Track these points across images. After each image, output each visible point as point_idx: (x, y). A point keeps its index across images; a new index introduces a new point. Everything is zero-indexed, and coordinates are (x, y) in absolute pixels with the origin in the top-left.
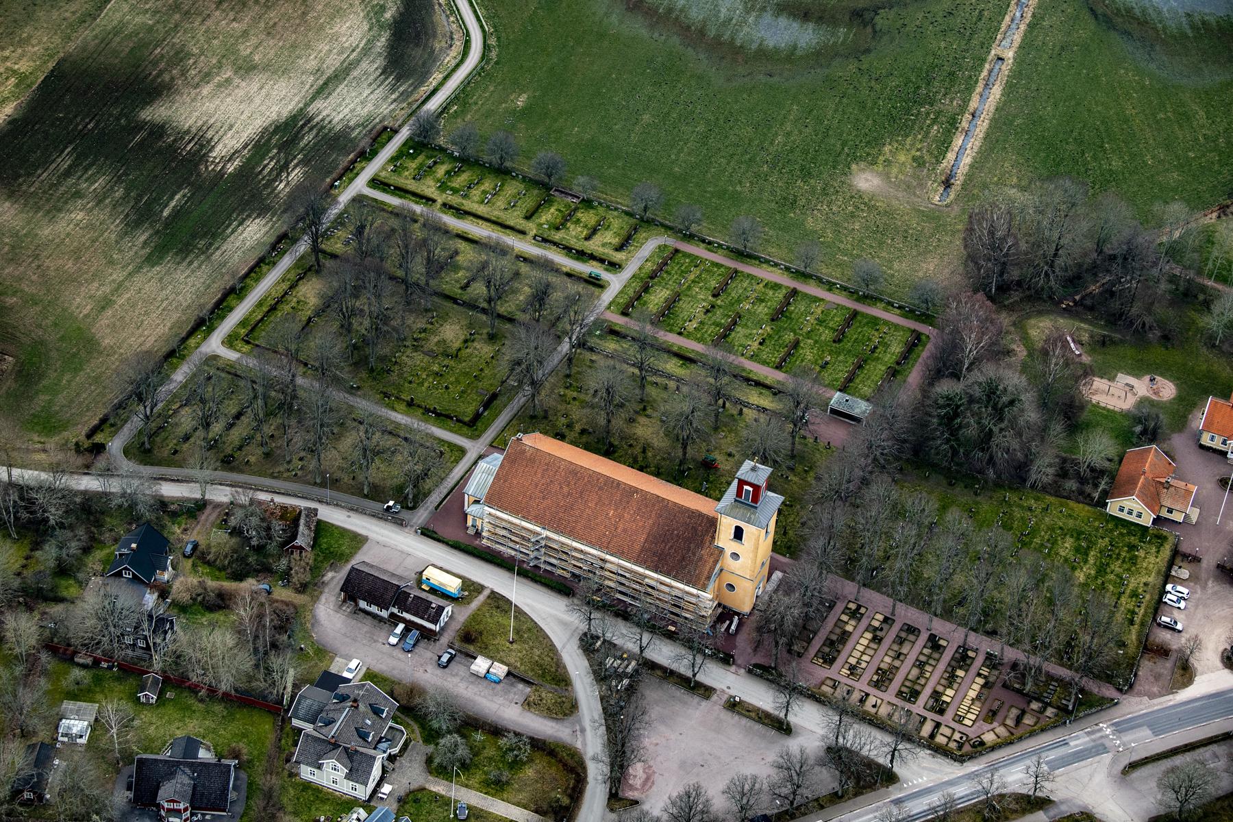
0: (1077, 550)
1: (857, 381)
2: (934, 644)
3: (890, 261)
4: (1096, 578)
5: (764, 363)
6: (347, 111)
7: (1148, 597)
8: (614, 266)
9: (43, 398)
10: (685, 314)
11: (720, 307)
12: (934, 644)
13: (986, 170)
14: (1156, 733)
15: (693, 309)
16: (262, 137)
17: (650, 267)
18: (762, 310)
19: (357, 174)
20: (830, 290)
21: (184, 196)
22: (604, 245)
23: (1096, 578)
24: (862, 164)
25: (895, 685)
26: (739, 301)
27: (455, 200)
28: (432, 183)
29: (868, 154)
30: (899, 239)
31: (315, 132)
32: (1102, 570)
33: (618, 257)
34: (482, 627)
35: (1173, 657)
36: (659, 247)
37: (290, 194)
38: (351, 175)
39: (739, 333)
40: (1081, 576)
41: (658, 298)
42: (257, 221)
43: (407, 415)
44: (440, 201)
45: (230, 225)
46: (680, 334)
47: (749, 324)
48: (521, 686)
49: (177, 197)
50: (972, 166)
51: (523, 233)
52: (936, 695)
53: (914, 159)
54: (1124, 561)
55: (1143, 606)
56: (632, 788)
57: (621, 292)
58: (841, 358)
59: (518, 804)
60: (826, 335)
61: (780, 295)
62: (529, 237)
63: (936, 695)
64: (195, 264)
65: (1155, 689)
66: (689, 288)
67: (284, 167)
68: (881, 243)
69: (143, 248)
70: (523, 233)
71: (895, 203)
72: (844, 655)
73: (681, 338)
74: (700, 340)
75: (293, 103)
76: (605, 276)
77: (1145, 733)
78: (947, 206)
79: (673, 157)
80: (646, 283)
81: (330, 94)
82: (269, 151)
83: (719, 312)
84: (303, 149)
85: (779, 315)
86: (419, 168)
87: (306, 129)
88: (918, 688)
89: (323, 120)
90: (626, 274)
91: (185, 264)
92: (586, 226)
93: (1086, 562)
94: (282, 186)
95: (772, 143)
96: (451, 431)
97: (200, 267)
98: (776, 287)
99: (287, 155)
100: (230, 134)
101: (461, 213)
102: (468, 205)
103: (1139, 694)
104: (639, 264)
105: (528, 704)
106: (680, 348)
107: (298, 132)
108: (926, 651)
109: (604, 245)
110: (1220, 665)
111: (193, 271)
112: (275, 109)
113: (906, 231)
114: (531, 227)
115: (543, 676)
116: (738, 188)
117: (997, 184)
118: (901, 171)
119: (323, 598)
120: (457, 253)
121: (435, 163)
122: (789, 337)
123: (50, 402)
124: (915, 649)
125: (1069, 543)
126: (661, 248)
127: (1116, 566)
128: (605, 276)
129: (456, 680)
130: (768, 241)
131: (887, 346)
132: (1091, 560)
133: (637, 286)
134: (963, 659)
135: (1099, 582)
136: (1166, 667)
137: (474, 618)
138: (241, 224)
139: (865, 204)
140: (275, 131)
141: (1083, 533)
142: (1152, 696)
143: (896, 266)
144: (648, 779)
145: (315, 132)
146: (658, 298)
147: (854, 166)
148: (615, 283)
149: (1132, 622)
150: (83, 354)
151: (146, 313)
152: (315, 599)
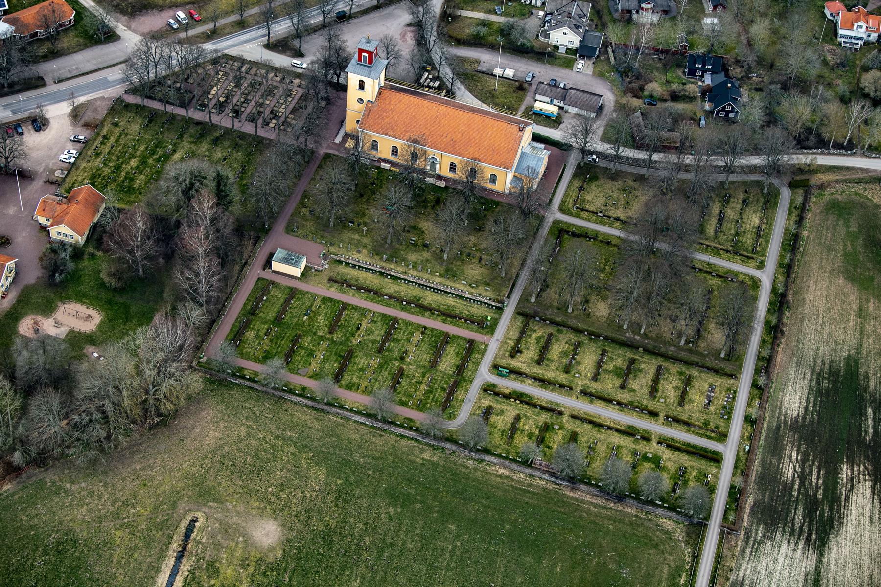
0: (132, 180)
1: (282, 300)
2: (237, 113)
3: (249, 435)
4: (122, 163)
5: (355, 308)
6: (781, 560)
7: (89, 153)
8: (488, 389)
9: (854, 229)
10: (425, 347)
11: (396, 359)
12: (237, 113)
13: (144, 567)
14: (105, 78)
15: (418, 354)
16: (839, 511)
17: (460, 394)
18: (361, 361)
19: (736, 467)
20: (304, 389)
21: (866, 432)
22: (502, 412)
23: (122, 163)
24: (271, 558)
25: (263, 88)
26: (381, 366)
27: (642, 447)
28: (669, 464)
29: (264, 574)
30: (239, 464)
31: (797, 527)
32: (118, 168)
33: (487, 402)
34: (515, 95)
35: (82, 122)
36: (455, 417)
37: (783, 449)
38: (740, 465)
39: (378, 334)
40: (134, 163)
41: (449, 361)
42: (795, 414)
43: (608, 235)
44: (654, 444)
45: (815, 406)
46: (426, 328)
47: (370, 345)
48: (484, 70)
49: (871, 430)
50: (158, 570)
51: (574, 417)
52: (238, 85)
53: (217, 572)
54: (100, 175)
55: (94, 147)
56: (412, 32)
57: (478, 364)
58: (295, 320)
59: (470, 18)
60: (307, 341)
61: (346, 378)
62: (567, 413)
63: (238, 85)
64: (819, 361)
65: (99, 103)
66: (424, 375)
67: (803, 477)
68: (256, 456)
69: (867, 373)
70: (574, 417)
71: (241, 508)
72: (295, 101)
73: (424, 324)
74: (408, 324)
75: (833, 562)
76: (494, 379)
77: (110, 79)
78: (190, 511)
79: (459, 544)
80: (461, 376)
81: (806, 580)
82: (824, 495)
83: (396, 354)
84: (797, 502)
85: (346, 358)
86: (685, 482)
87: (806, 529)
88: (250, 89)
89: (797, 544)
90: (475, 389)
91: (827, 361)
92: (522, 431)
93: (127, 173)
94: (794, 455)
95: (363, 578)
96: (573, 225)
97: (815, 359)
98: (350, 387)
99: (807, 494)
100: (868, 514)
101: (629, 432)
102: (626, 442)
103: (111, 98)
104: (469, 395)
105: (478, 62)
106: (423, 316)
107: (810, 524)
108: (243, 109)
109: (502, 412)
110: (51, 121)
111: (817, 354)
112: (845, 551)
113: (232, 473)
114: (570, 425)
115: (473, 76)
116: (391, 510)
117: (136, 548)
118: (233, 551)
119: (613, 104)
120: (622, 387)
121: (674, 491)
122: (337, 336)
123: (848, 227)
124: (249, 109)
125: (137, 184)
126: (452, 416)
127: (106, 171)
128: (494, 379)
129: (521, 69)
130: (360, 447)
131: (257, 337)
132: (123, 174)
133: (467, 373)
134: (221, 106)
135: (121, 160)
136: (89, 116)
137: (521, 100)
138: (806, 408)
139: (269, 503)
140: (831, 519)
141: (125, 192)
142: (103, 98)
143: (243, 431)
144: (404, 36)
145: (797, 527)
146: (449, 361)
147: (279, 554)
148: (484, 374)
149: (105, 137)
150: (850, 268)
151: (828, 309)
152: (616, 102)
